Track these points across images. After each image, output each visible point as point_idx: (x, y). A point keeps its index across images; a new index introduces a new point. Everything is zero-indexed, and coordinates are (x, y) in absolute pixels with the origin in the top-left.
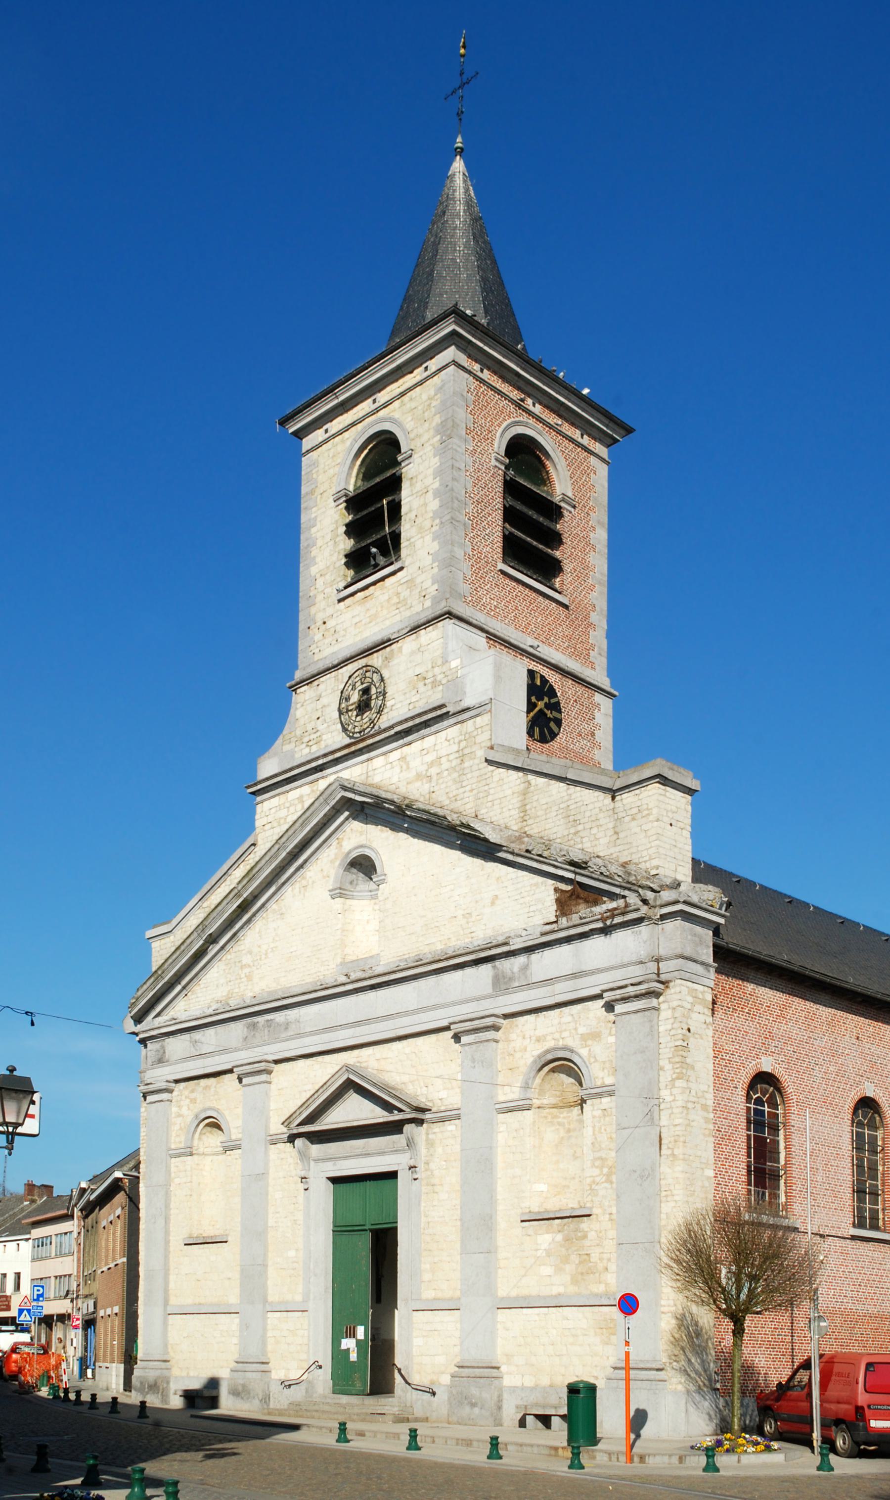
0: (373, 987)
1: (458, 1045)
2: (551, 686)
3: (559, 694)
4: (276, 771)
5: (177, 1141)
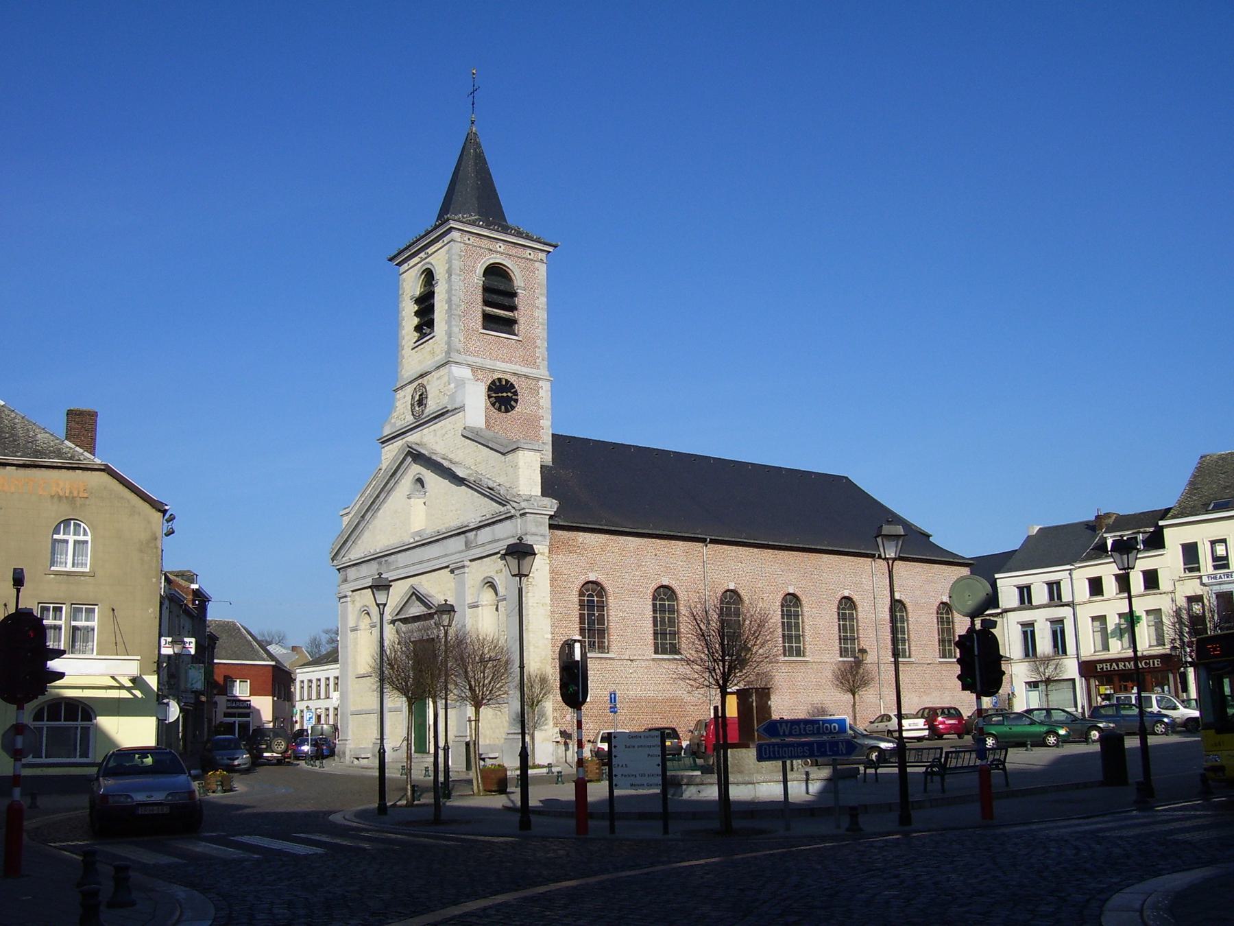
0: (423, 545)
1: (452, 575)
2: (511, 384)
3: (516, 387)
4: (389, 433)
5: (351, 624)
